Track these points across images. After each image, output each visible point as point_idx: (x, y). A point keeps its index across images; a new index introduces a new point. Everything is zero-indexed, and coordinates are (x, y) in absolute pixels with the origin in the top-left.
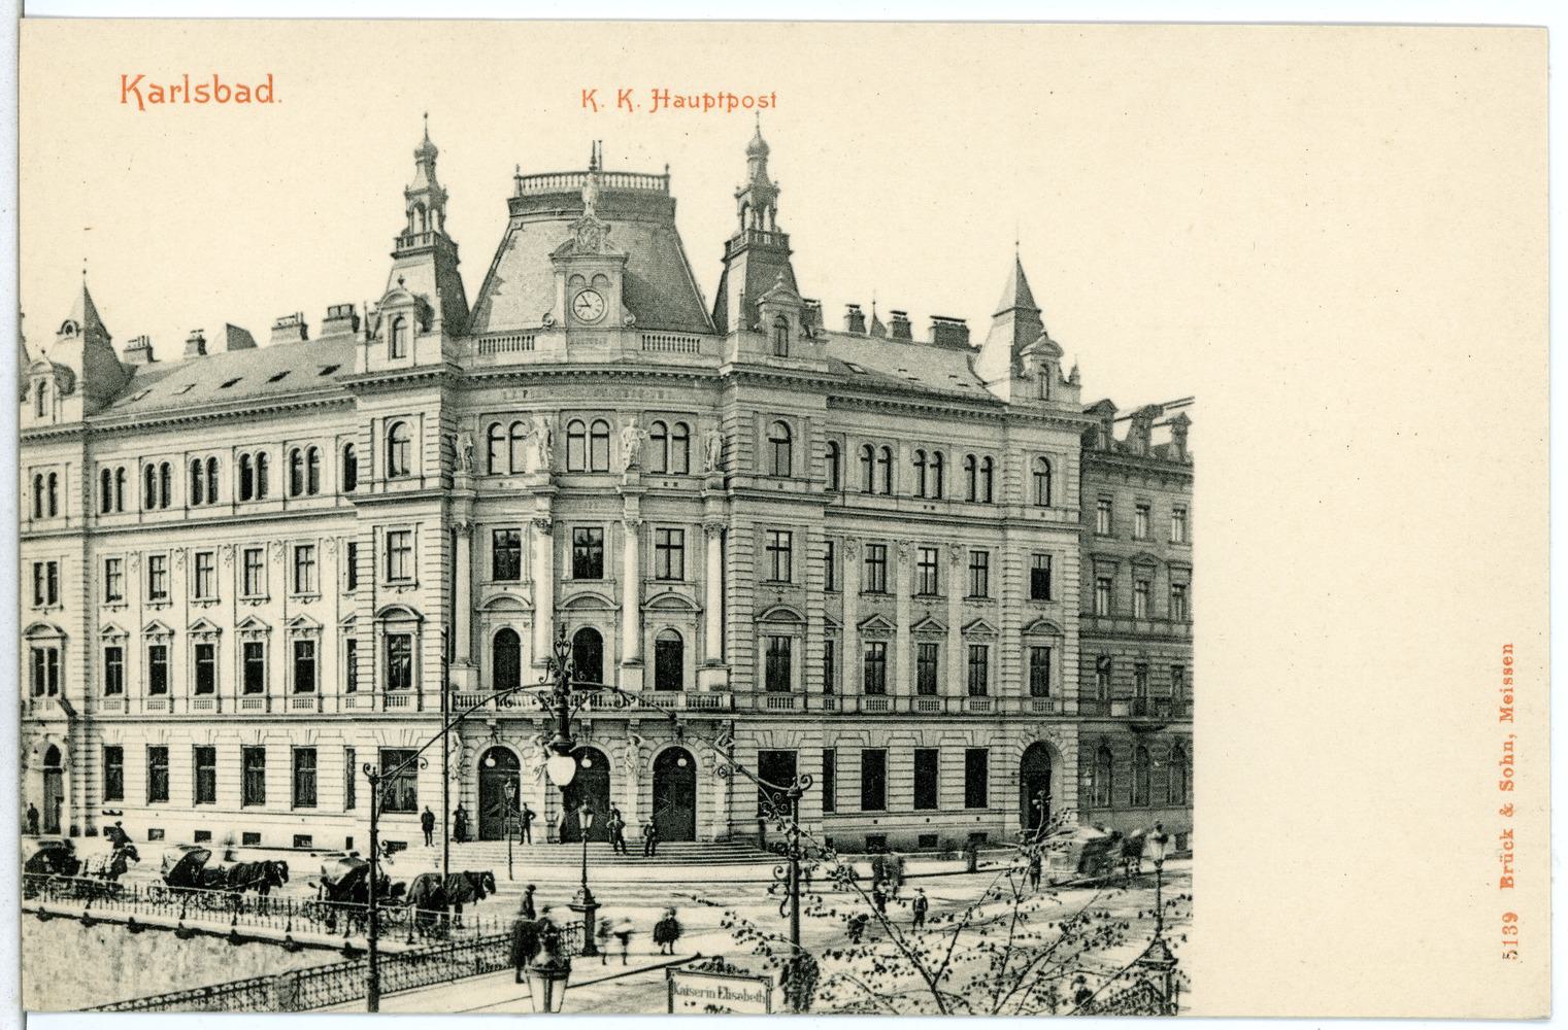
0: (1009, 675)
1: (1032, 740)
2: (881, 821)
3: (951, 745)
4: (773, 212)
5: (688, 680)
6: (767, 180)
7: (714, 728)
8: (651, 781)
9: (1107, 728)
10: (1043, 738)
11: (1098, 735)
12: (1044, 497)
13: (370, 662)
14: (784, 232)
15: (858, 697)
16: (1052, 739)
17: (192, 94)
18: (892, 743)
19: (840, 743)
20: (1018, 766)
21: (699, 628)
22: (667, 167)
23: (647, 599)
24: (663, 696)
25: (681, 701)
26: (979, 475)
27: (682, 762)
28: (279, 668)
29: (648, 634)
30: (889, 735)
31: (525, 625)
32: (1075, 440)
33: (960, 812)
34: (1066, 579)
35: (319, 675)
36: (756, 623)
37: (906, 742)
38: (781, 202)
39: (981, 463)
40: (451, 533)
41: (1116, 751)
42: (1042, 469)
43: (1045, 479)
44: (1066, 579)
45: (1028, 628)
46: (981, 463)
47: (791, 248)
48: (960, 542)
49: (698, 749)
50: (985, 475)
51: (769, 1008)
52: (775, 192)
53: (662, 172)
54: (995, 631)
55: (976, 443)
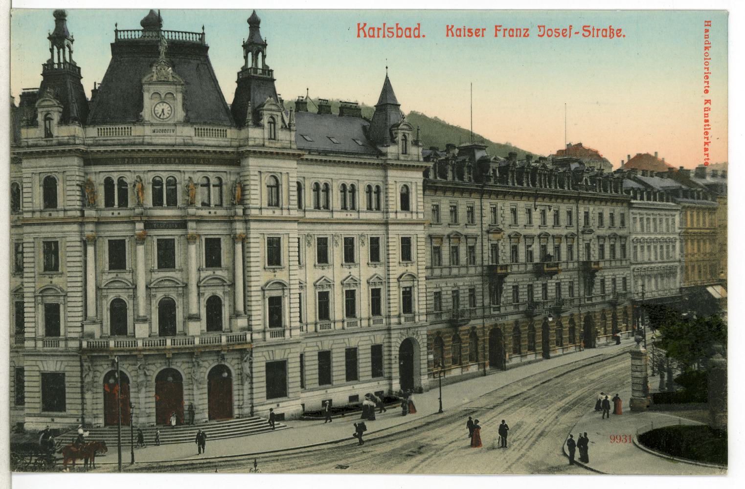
0: (393, 301)
1: (404, 338)
2: (356, 387)
3: (363, 345)
4: (264, 57)
5: (225, 324)
6: (261, 39)
7: (242, 353)
8: (206, 386)
9: (439, 326)
10: (410, 336)
11: (435, 331)
12: (274, 200)
13: (420, 299)
14: (270, 68)
15: (399, 316)
16: (414, 337)
17: (386, 33)
18: (334, 346)
19: (307, 349)
20: (398, 353)
21: (185, 294)
22: (203, 28)
23: (201, 278)
24: (214, 335)
25: (224, 339)
26: (348, 194)
27: (226, 374)
28: (337, 308)
29: (202, 299)
30: (331, 342)
31: (129, 296)
32: (419, 176)
33: (369, 381)
34: (34, 257)
35: (316, 313)
36: (399, 281)
37: (340, 346)
38: (268, 51)
39: (374, 189)
40: (85, 243)
41: (445, 338)
42: (273, 182)
43: (274, 189)
44: (34, 257)
45: (401, 277)
46: (374, 189)
47: (368, 97)
48: (312, 233)
49: (232, 363)
50: (325, 193)
51: (476, 442)
52: (265, 45)
53: (201, 32)
54: (384, 280)
55: (346, 177)
